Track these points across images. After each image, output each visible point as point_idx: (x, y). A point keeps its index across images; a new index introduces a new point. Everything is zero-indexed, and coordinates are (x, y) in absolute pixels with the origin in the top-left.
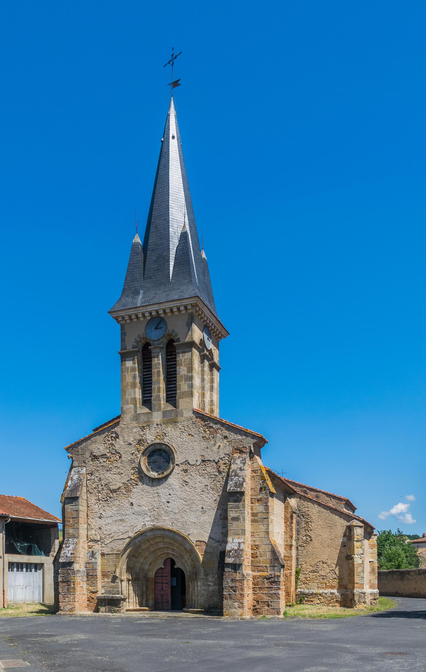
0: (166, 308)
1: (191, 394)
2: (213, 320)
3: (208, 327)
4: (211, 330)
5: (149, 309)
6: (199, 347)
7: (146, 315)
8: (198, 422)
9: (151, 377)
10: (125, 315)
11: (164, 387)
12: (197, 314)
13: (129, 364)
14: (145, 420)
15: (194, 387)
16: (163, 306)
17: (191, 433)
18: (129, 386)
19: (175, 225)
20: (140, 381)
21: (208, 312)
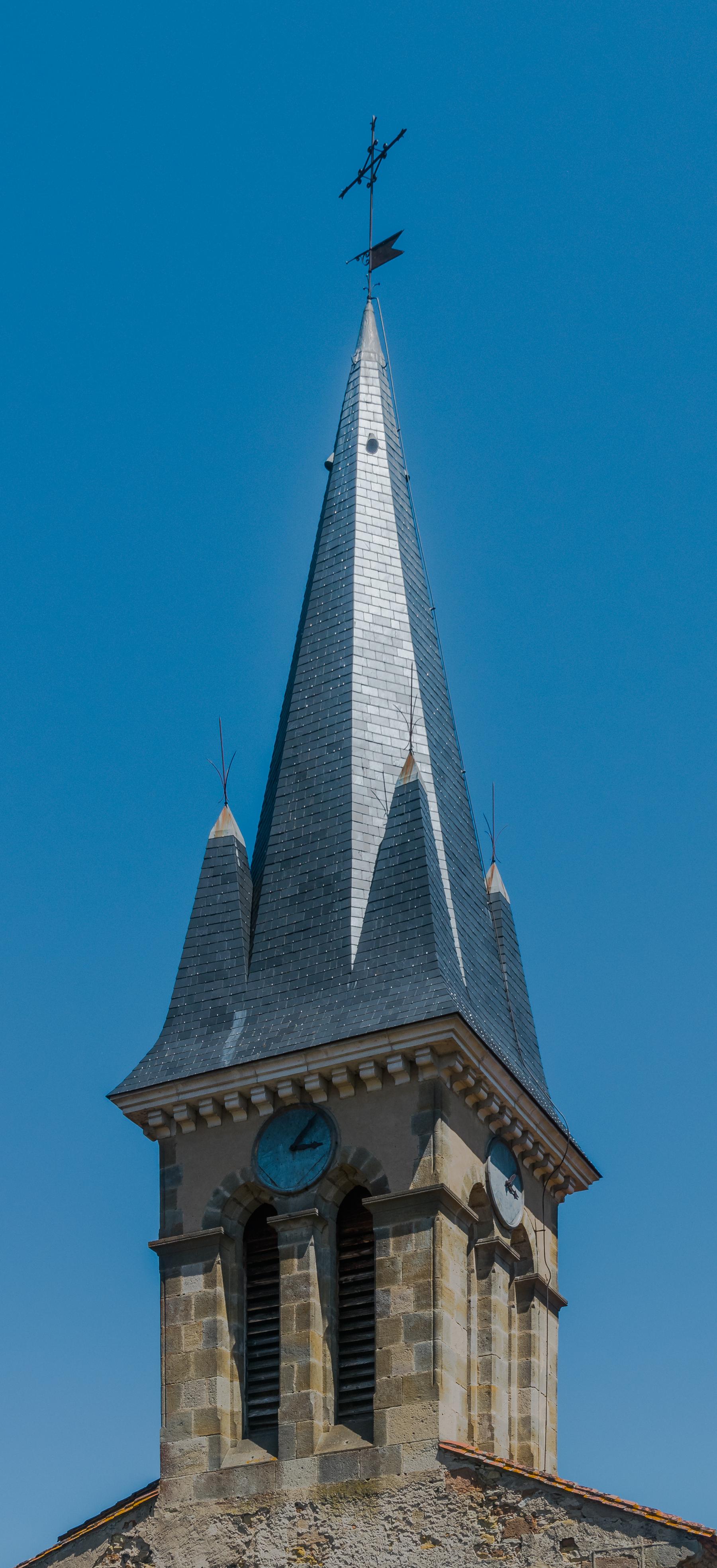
0: (331, 1069)
1: (431, 1388)
2: (530, 1117)
3: (509, 1144)
4: (523, 1155)
5: (268, 1074)
6: (464, 1212)
7: (254, 1099)
8: (461, 1490)
9: (277, 1333)
10: (176, 1105)
11: (329, 1365)
12: (457, 1087)
13: (192, 1285)
14: (254, 1490)
15: (445, 1359)
16: (321, 1062)
17: (429, 1533)
18: (192, 1368)
19: (373, 765)
20: (235, 1348)
21: (506, 1080)
